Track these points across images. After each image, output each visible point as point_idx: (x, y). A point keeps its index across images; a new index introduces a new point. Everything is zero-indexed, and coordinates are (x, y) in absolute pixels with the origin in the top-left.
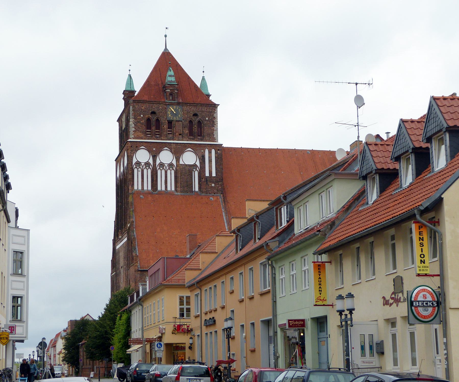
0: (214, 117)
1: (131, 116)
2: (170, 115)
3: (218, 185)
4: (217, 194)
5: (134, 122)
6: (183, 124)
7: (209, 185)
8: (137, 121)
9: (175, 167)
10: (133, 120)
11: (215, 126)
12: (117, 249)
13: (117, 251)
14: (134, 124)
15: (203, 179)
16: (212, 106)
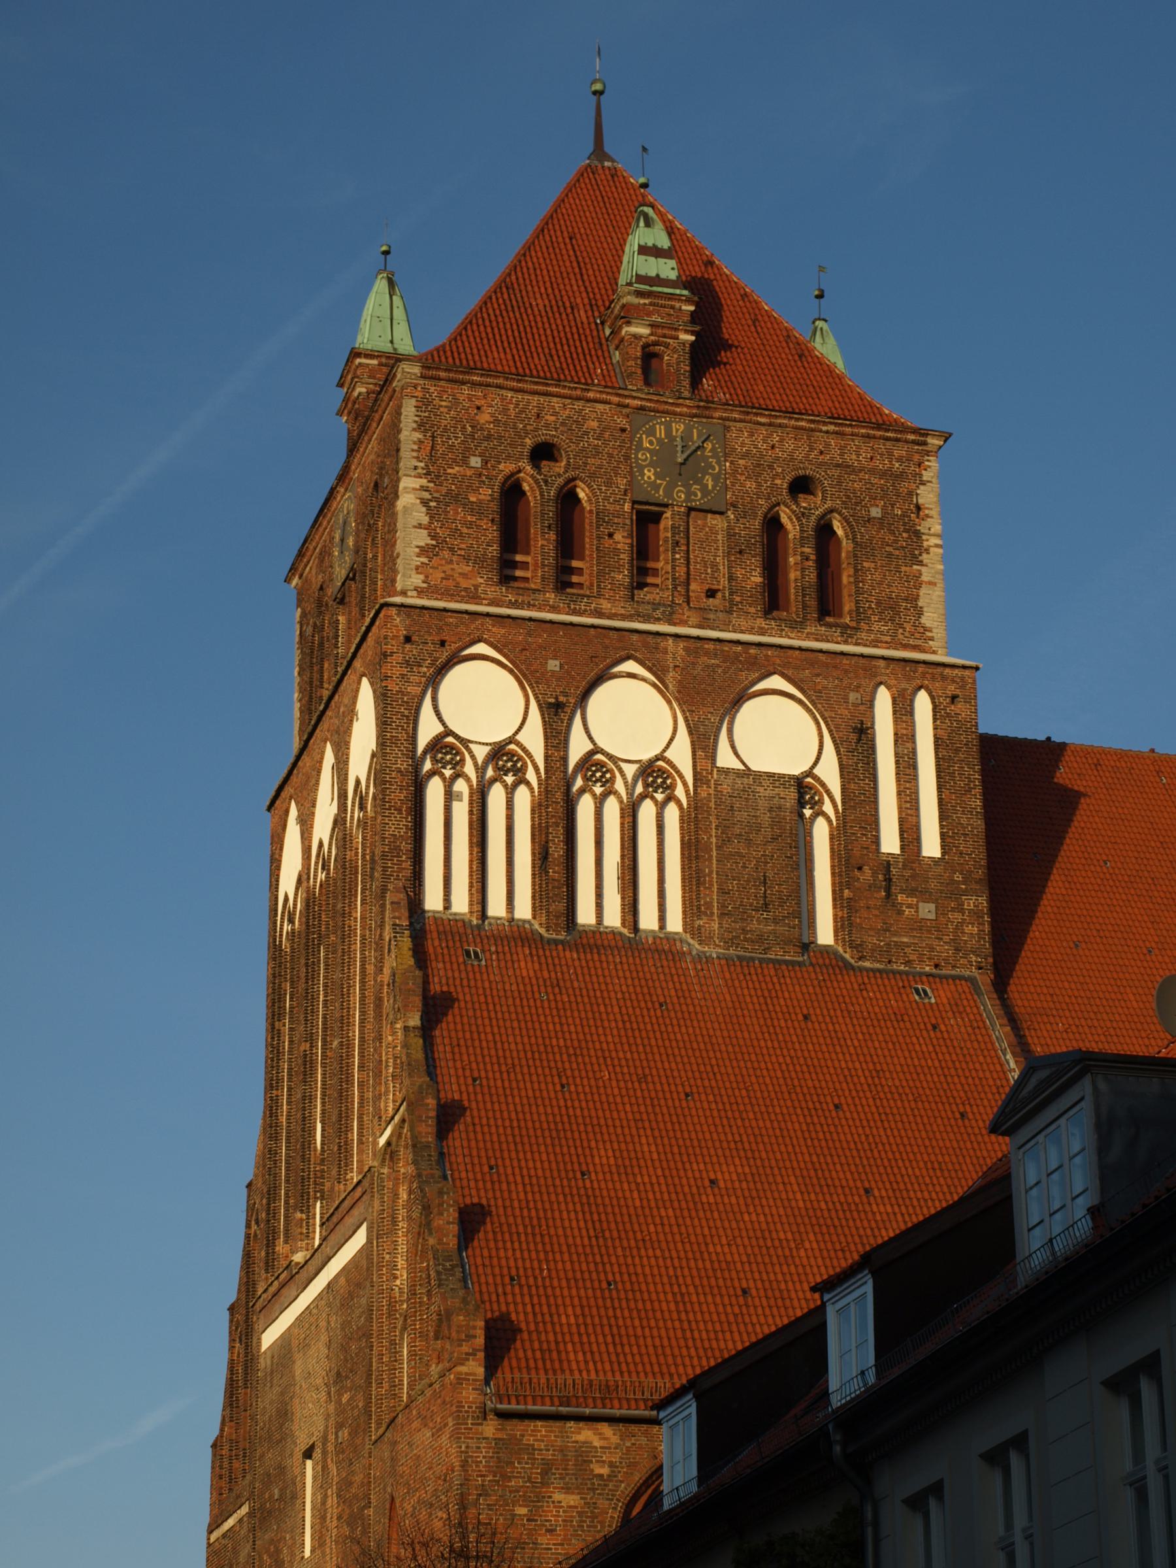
0: (918, 508)
1: (408, 458)
2: (649, 474)
3: (962, 911)
4: (954, 967)
5: (427, 495)
6: (730, 534)
7: (900, 913)
8: (444, 490)
9: (685, 784)
10: (424, 482)
11: (925, 557)
12: (263, 1349)
13: (264, 1363)
14: (429, 508)
15: (860, 869)
16: (907, 441)
